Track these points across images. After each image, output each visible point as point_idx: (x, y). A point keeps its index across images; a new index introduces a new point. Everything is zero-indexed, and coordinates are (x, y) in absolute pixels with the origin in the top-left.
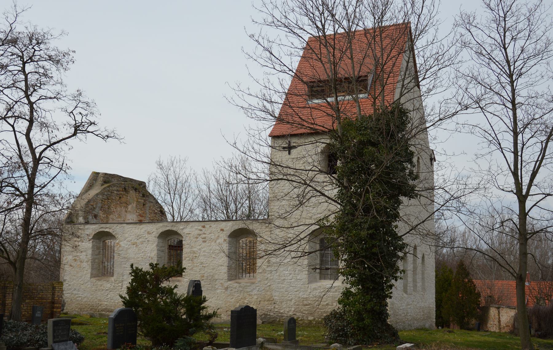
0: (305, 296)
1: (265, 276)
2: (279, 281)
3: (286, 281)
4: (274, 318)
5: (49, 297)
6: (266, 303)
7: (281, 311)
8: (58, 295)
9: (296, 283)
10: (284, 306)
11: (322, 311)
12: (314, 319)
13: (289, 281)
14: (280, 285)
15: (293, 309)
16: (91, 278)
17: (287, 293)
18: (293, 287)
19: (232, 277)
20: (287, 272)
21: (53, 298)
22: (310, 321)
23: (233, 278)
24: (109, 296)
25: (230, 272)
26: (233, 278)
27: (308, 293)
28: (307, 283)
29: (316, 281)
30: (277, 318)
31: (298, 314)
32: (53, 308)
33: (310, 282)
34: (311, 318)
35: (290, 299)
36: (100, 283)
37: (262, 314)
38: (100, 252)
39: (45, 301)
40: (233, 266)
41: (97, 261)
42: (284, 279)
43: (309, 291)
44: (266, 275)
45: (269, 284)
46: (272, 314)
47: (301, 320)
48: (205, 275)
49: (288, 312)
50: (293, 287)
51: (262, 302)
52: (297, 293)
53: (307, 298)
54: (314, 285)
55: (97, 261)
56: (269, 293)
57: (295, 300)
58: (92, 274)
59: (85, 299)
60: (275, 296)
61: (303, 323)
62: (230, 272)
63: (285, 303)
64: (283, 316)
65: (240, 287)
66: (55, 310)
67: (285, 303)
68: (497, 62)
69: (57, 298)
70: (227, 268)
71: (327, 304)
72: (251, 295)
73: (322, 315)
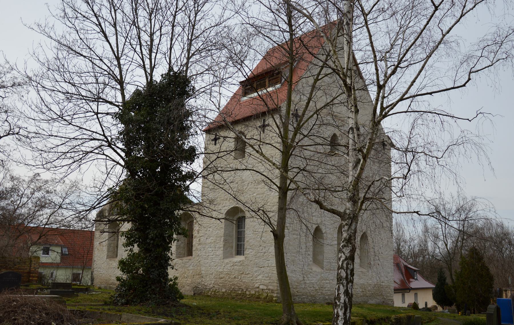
0: (221, 270)
1: (197, 253)
2: (205, 257)
3: (210, 257)
4: (201, 290)
5: (27, 268)
6: (198, 277)
7: (206, 284)
8: (34, 267)
9: (216, 258)
10: (208, 280)
11: (231, 283)
12: (226, 291)
13: (211, 257)
14: (205, 261)
15: (213, 282)
16: (107, 259)
17: (210, 267)
18: (214, 262)
19: (180, 255)
20: (210, 249)
21: (30, 269)
22: (223, 293)
23: (181, 256)
24: (115, 272)
25: (179, 251)
26: (181, 256)
27: (222, 267)
28: (222, 258)
29: (232, 257)
30: (203, 290)
31: (216, 286)
32: (30, 277)
33: (225, 257)
34: (224, 290)
35: (211, 273)
36: (111, 263)
37: (194, 286)
38: (115, 238)
39: (22, 271)
40: (181, 245)
41: (112, 245)
42: (208, 255)
43: (224, 265)
44: (197, 252)
45: (199, 260)
46: (200, 287)
47: (218, 292)
48: (361, 290)
49: (210, 285)
50: (214, 262)
51: (195, 276)
52: (216, 267)
53: (222, 272)
54: (227, 261)
55: (112, 245)
56: (199, 268)
57: (215, 274)
58: (107, 256)
59: (103, 276)
60: (203, 271)
61: (219, 294)
62: (179, 251)
63: (208, 276)
64: (206, 289)
65: (183, 263)
66: (31, 278)
67: (208, 276)
68: (443, 236)
69: (34, 269)
70: (175, 247)
71: (235, 278)
72: (188, 270)
73: (231, 288)
